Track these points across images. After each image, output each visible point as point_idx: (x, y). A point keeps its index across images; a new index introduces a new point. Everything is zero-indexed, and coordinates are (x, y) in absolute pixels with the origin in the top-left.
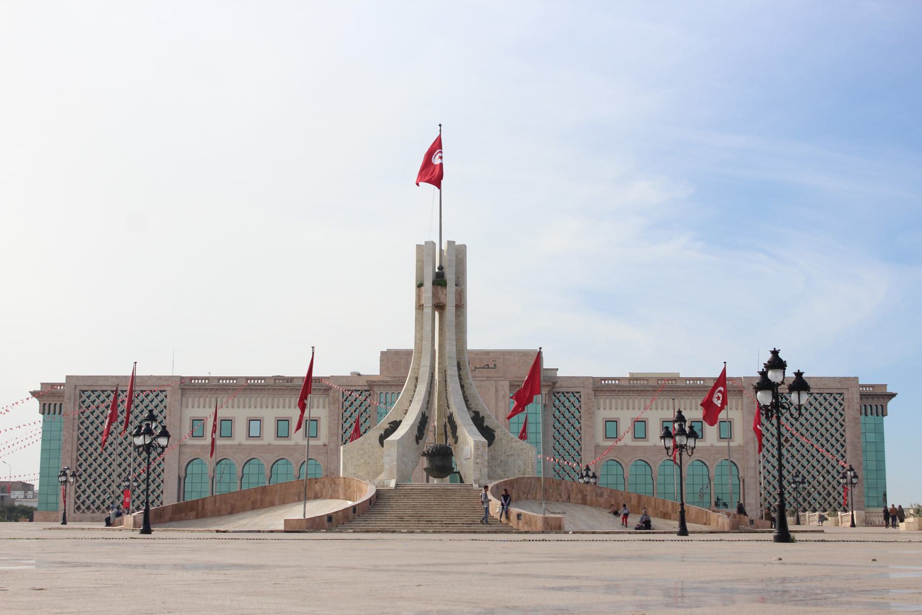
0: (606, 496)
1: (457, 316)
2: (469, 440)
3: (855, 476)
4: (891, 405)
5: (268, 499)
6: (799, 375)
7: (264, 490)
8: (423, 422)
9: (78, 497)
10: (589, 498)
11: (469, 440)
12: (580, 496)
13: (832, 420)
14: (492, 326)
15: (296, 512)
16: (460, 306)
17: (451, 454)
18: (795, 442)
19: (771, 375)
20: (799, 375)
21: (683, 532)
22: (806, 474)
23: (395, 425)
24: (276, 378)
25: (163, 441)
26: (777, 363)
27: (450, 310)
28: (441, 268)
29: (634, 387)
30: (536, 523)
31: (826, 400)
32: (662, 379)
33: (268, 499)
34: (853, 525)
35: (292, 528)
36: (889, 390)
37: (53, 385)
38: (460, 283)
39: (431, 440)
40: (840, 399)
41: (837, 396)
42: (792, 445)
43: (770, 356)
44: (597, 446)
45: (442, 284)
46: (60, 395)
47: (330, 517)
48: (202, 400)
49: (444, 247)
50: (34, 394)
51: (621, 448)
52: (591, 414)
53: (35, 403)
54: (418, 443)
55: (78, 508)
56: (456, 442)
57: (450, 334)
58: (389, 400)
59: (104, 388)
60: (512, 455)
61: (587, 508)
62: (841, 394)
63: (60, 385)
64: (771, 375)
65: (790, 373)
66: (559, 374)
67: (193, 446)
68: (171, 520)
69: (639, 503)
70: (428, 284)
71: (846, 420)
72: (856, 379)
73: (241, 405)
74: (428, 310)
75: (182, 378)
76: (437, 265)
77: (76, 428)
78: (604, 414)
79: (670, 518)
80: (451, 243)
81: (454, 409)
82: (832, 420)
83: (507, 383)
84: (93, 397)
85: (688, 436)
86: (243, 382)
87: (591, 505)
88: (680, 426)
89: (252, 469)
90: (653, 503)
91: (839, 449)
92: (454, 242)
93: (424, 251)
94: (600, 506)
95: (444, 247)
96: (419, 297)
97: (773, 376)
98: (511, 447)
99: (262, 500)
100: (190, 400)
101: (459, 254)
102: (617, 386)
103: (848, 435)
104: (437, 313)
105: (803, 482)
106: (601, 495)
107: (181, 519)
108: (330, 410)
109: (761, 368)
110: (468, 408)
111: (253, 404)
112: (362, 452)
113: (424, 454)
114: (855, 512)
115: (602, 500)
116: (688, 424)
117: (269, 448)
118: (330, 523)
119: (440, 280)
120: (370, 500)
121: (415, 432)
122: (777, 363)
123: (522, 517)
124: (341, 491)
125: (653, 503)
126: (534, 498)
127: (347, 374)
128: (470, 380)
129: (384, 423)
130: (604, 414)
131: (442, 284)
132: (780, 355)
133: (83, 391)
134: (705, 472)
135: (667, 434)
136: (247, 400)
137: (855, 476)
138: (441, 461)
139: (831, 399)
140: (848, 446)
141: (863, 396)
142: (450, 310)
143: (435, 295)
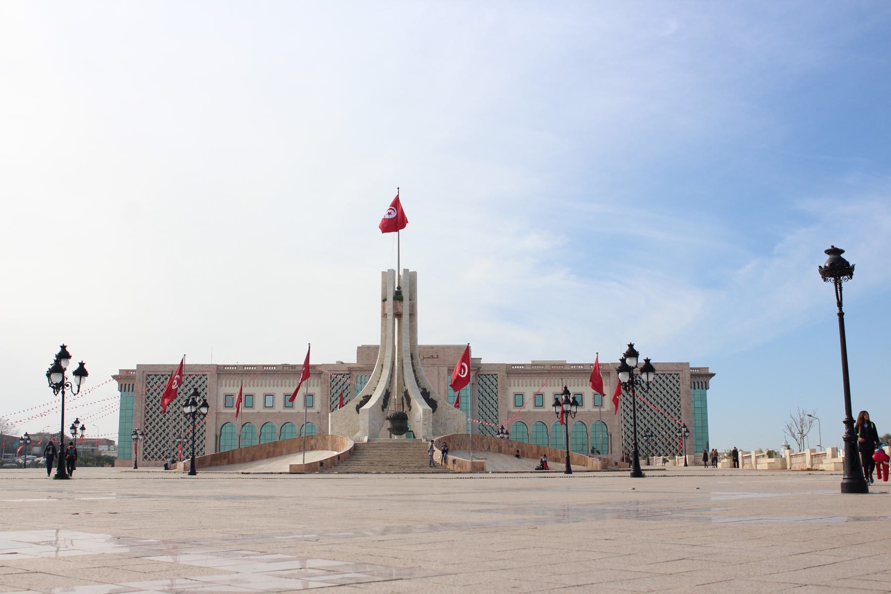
1: (411, 321)
2: (419, 408)
3: (687, 431)
4: (712, 382)
5: (278, 450)
6: (647, 361)
7: (275, 444)
8: (387, 395)
9: (146, 450)
11: (419, 408)
12: (497, 447)
14: (433, 330)
15: (298, 460)
16: (413, 315)
17: (407, 418)
18: (646, 408)
19: (628, 361)
20: (647, 361)
21: (569, 471)
22: (654, 430)
23: (367, 398)
26: (632, 353)
28: (399, 288)
33: (278, 450)
34: (686, 465)
35: (295, 471)
37: (127, 371)
39: (392, 409)
40: (677, 378)
42: (644, 410)
44: (509, 412)
45: (400, 299)
46: (133, 378)
47: (321, 463)
49: (401, 273)
50: (115, 377)
51: (525, 413)
52: (505, 390)
53: (115, 384)
55: (146, 457)
56: (410, 410)
61: (502, 455)
63: (133, 371)
65: (641, 360)
66: (482, 362)
67: (226, 413)
68: (210, 465)
69: (538, 451)
72: (688, 364)
74: (390, 317)
75: (218, 366)
76: (397, 286)
80: (406, 271)
81: (408, 387)
84: (156, 379)
85: (572, 405)
86: (241, 369)
87: (505, 453)
88: (566, 397)
93: (387, 276)
95: (401, 273)
99: (274, 452)
101: (412, 278)
103: (682, 403)
106: (512, 446)
107: (217, 465)
113: (388, 419)
116: (572, 396)
119: (398, 296)
120: (350, 451)
121: (382, 403)
122: (632, 353)
124: (329, 445)
127: (333, 361)
128: (420, 367)
129: (359, 397)
130: (513, 390)
131: (400, 299)
134: (585, 429)
137: (687, 431)
138: (400, 423)
140: (682, 411)
142: (406, 317)
143: (395, 307)
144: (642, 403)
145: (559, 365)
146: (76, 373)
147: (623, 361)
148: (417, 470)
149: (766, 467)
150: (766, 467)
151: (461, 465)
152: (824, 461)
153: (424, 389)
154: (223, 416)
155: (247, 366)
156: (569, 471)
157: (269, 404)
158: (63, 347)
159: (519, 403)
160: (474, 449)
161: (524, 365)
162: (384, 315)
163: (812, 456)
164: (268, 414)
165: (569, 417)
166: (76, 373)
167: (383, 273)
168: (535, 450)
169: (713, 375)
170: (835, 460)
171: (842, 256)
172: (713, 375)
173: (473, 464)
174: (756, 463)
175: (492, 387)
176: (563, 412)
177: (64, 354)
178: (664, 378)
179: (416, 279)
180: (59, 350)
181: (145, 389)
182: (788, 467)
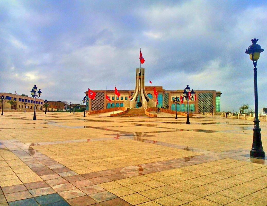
2: (144, 100)
3: (213, 107)
5: (111, 110)
6: (192, 90)
7: (110, 109)
8: (137, 98)
11: (144, 100)
15: (112, 113)
19: (187, 90)
20: (192, 90)
23: (132, 98)
26: (188, 88)
27: (142, 79)
28: (140, 72)
34: (213, 115)
36: (221, 93)
39: (138, 101)
43: (187, 86)
47: (118, 114)
49: (141, 69)
52: (170, 96)
57: (142, 84)
64: (187, 90)
65: (191, 90)
66: (165, 90)
68: (95, 113)
70: (138, 75)
72: (215, 91)
74: (138, 80)
75: (107, 91)
76: (140, 72)
78: (172, 96)
80: (142, 68)
84: (98, 93)
85: (178, 101)
88: (176, 99)
89: (117, 104)
93: (138, 70)
95: (141, 69)
96: (137, 77)
97: (187, 91)
101: (143, 70)
104: (140, 80)
107: (97, 113)
109: (32, 88)
110: (144, 96)
113: (137, 103)
114: (213, 113)
117: (119, 101)
118: (118, 115)
119: (140, 74)
121: (135, 99)
122: (188, 88)
124: (122, 109)
132: (189, 86)
135: (174, 101)
137: (213, 107)
138: (140, 104)
141: (216, 93)
142: (142, 79)
143: (139, 77)
146: (38, 92)
148: (141, 116)
149: (232, 118)
150: (232, 118)
151: (151, 115)
152: (249, 117)
153: (146, 96)
158: (35, 86)
161: (175, 91)
163: (245, 116)
164: (117, 101)
165: (177, 104)
166: (38, 92)
167: (137, 69)
169: (222, 93)
170: (252, 117)
171: (247, 50)
172: (222, 93)
173: (154, 115)
174: (230, 116)
175: (167, 96)
176: (176, 103)
177: (35, 87)
179: (144, 70)
180: (34, 86)
182: (239, 118)
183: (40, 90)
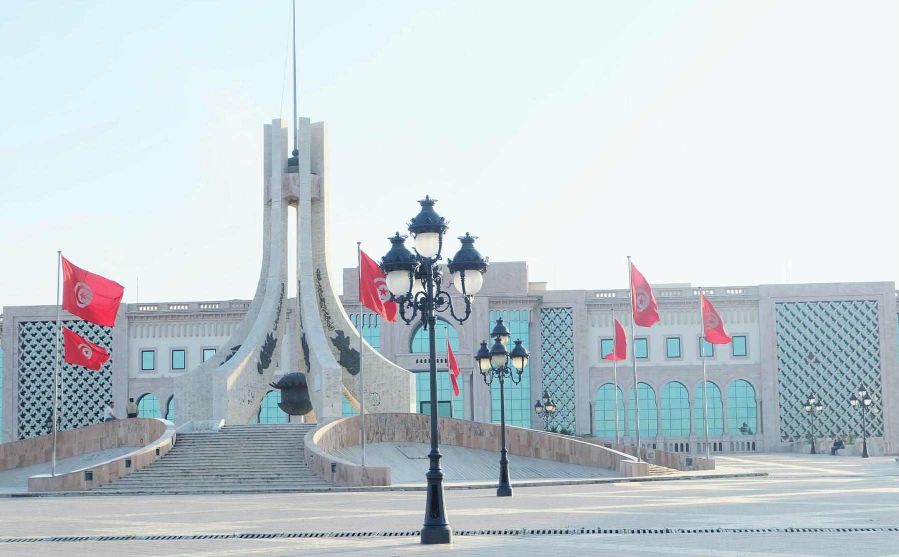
0: (488, 435)
8: (270, 346)
10: (465, 437)
12: (453, 435)
13: (864, 331)
16: (317, 200)
18: (820, 358)
22: (822, 394)
24: (231, 303)
25: (517, 363)
26: (428, 222)
28: (295, 153)
29: (667, 298)
30: (352, 476)
31: (845, 308)
32: (668, 290)
38: (316, 170)
41: (870, 304)
42: (817, 361)
44: (592, 369)
48: (151, 328)
54: (261, 372)
56: (308, 371)
58: (373, 322)
59: (45, 319)
60: (383, 384)
61: (462, 450)
62: (875, 301)
66: (548, 288)
67: (143, 380)
69: (529, 443)
71: (880, 331)
73: (163, 334)
76: (291, 149)
77: (17, 364)
79: (568, 462)
80: (305, 121)
82: (864, 331)
83: (486, 300)
86: (196, 307)
87: (468, 447)
90: (547, 442)
91: (873, 364)
92: (308, 119)
94: (480, 448)
98: (383, 375)
100: (138, 329)
101: (313, 136)
102: (612, 299)
105: (819, 404)
108: (292, 336)
110: (330, 327)
111: (182, 333)
112: (198, 386)
115: (482, 440)
122: (428, 222)
123: (336, 469)
125: (547, 442)
126: (392, 440)
133: (23, 324)
134: (717, 394)
136: (182, 327)
139: (863, 307)
144: (813, 350)
145: (673, 290)
147: (397, 241)
154: (137, 385)
155: (204, 303)
156: (504, 490)
157: (148, 365)
159: (674, 352)
160: (410, 440)
162: (268, 203)
165: (507, 381)
168: (523, 441)
178: (851, 307)
181: (17, 345)
183: (467, 241)
